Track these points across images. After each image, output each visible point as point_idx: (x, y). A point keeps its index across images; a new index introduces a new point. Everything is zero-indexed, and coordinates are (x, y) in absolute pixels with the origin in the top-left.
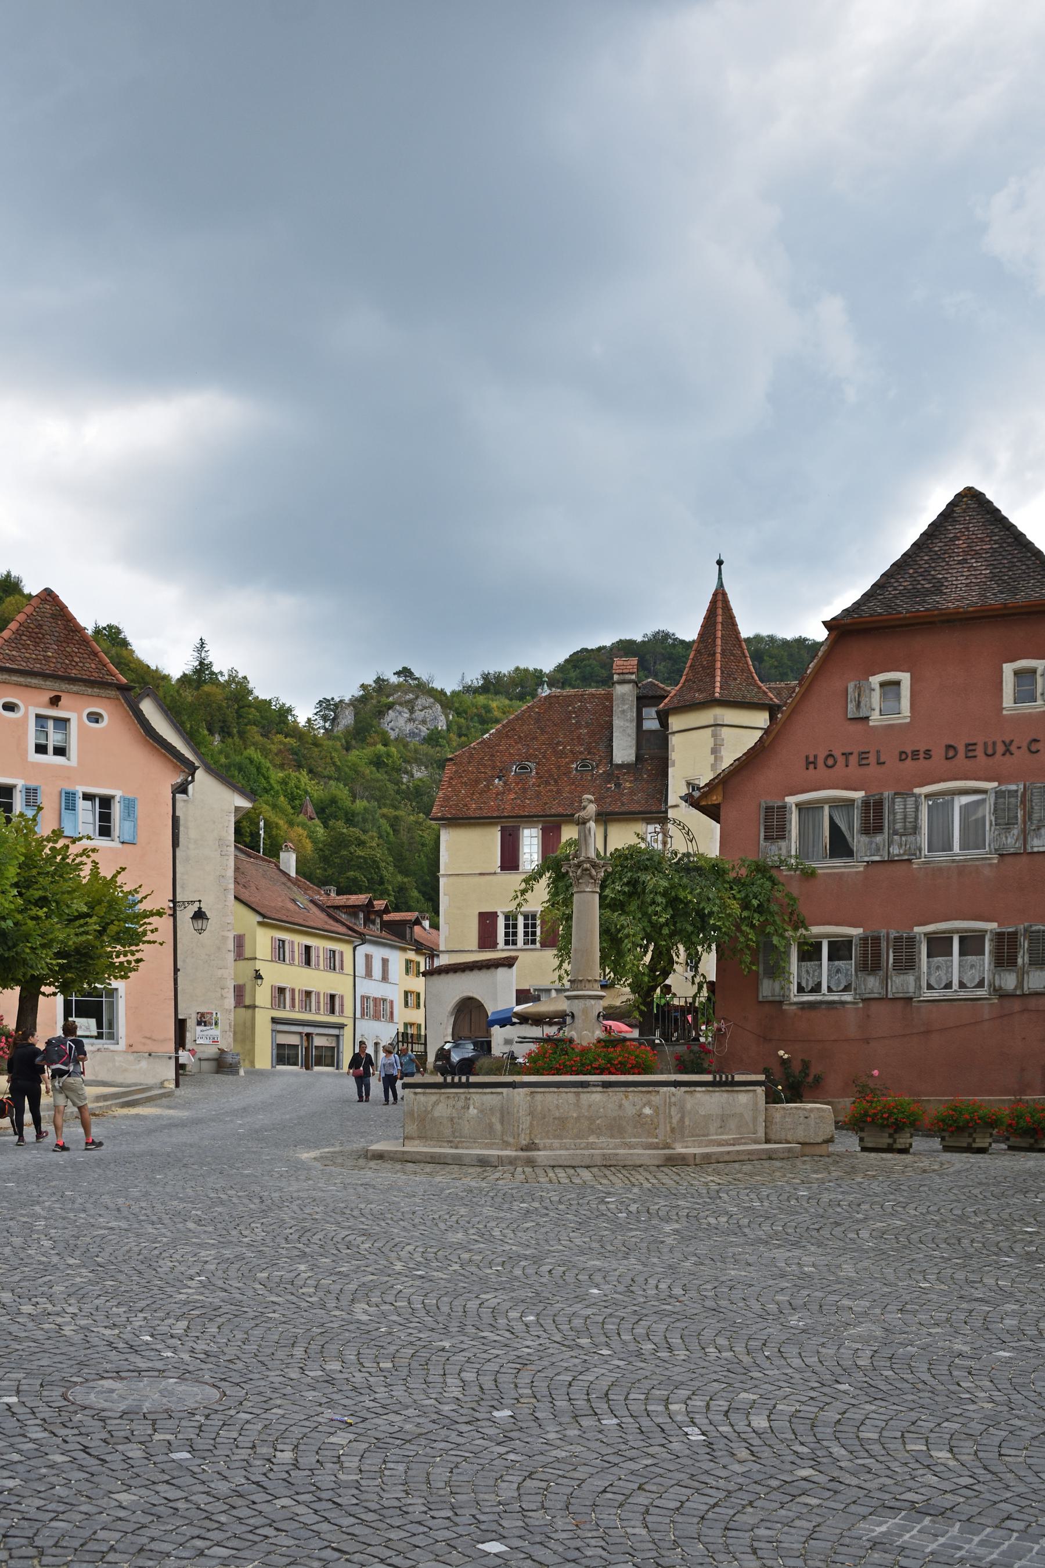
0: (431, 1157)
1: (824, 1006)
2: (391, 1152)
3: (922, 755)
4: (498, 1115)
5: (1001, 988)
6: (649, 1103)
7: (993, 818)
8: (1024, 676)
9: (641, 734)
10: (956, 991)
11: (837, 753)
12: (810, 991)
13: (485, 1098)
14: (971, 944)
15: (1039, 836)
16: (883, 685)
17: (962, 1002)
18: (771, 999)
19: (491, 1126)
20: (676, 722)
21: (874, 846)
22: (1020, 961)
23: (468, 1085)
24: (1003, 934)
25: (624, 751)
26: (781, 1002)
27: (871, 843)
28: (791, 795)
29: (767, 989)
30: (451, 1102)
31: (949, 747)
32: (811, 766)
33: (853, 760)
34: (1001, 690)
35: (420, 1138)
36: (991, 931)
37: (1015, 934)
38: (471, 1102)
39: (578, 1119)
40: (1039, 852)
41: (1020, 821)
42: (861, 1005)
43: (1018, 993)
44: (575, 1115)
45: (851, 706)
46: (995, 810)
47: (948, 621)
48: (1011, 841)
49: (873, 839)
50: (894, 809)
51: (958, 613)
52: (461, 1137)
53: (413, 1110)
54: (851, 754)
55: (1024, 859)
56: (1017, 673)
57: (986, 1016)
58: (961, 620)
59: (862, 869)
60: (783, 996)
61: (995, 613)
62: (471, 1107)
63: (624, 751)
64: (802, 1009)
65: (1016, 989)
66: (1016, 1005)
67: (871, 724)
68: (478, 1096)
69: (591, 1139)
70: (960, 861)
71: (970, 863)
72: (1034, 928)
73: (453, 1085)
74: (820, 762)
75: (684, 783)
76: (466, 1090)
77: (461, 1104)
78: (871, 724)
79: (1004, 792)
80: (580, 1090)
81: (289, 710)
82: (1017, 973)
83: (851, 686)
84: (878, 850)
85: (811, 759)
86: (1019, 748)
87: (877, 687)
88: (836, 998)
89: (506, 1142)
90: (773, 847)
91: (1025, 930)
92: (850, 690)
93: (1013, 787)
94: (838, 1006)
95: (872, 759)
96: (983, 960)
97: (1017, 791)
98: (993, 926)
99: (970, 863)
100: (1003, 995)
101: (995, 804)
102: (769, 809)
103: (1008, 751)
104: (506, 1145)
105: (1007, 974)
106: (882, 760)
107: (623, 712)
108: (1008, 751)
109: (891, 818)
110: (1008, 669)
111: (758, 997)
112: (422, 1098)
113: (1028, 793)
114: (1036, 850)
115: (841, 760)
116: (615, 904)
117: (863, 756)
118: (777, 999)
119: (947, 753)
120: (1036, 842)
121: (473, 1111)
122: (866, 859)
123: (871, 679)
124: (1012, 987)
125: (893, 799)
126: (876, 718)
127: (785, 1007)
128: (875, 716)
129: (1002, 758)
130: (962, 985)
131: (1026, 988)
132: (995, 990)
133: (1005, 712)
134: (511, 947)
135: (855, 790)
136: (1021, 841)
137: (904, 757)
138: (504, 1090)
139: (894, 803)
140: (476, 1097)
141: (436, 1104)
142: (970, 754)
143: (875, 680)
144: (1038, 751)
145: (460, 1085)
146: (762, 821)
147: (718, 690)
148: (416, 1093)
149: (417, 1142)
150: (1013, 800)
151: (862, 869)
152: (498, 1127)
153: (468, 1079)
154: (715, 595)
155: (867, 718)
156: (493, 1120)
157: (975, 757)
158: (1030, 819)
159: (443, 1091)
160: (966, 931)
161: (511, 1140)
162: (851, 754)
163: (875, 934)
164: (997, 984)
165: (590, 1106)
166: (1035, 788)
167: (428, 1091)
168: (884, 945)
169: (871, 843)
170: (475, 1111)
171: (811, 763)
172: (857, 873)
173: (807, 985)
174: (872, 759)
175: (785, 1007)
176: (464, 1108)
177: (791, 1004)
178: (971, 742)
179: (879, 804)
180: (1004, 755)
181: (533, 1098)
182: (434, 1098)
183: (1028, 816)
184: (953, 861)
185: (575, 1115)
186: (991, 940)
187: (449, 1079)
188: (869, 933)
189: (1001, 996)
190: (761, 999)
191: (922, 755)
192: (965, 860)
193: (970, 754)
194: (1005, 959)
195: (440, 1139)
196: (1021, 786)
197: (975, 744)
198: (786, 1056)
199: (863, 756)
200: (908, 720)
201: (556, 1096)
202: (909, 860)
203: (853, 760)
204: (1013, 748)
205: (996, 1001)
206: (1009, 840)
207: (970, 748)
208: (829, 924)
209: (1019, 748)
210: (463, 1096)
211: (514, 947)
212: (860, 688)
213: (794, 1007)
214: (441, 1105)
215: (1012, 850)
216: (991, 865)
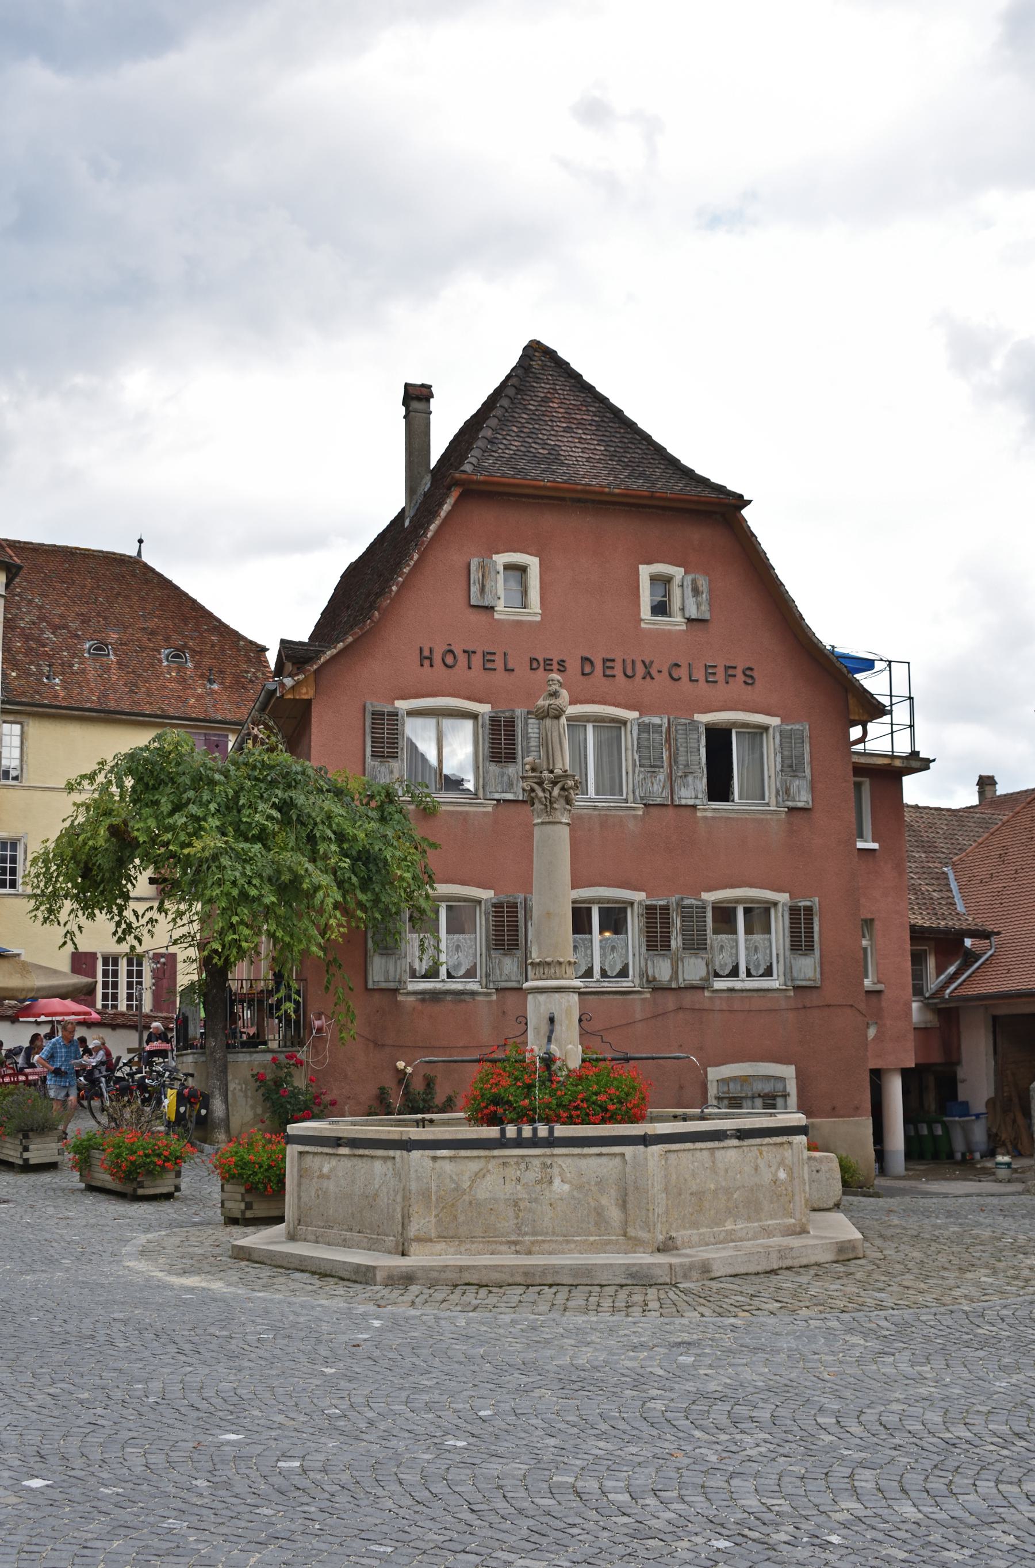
0: (526, 1274)
1: (449, 998)
2: (432, 1268)
4: (613, 1192)
5: (655, 979)
6: (782, 1163)
7: (636, 757)
10: (598, 981)
11: (458, 652)
12: (423, 977)
13: (583, 1163)
14: (614, 919)
15: (686, 785)
16: (508, 567)
17: (611, 997)
18: (383, 985)
19: (599, 1212)
21: (505, 778)
22: (673, 943)
23: (551, 1142)
26: (395, 991)
27: (502, 775)
28: (403, 699)
29: (379, 970)
30: (512, 1172)
31: (586, 660)
32: (427, 663)
33: (477, 660)
34: (638, 597)
35: (441, 1237)
36: (640, 903)
37: (666, 908)
38: (556, 1171)
39: (715, 1191)
40: (686, 806)
41: (665, 764)
42: (494, 997)
43: (674, 986)
44: (712, 1187)
45: (475, 589)
46: (639, 747)
47: (579, 500)
48: (657, 789)
49: (505, 770)
50: (528, 733)
51: (602, 493)
52: (534, 1234)
53: (429, 1189)
54: (474, 652)
55: (671, 811)
56: (654, 579)
57: (638, 1016)
58: (593, 501)
59: (490, 809)
60: (400, 982)
61: (667, 504)
62: (557, 1181)
64: (423, 1000)
65: (670, 981)
66: (670, 1002)
67: (496, 616)
68: (569, 1160)
69: (729, 1226)
70: (603, 808)
71: (613, 813)
72: (686, 902)
73: (519, 1142)
74: (437, 658)
76: (547, 1151)
77: (531, 1176)
78: (496, 616)
79: (648, 725)
80: (716, 1144)
81: (741, 502)
82: (672, 959)
83: (474, 563)
84: (511, 785)
85: (426, 653)
86: (659, 672)
87: (501, 569)
88: (459, 987)
89: (635, 1239)
90: (383, 769)
91: (677, 904)
92: (473, 568)
93: (656, 720)
94: (467, 998)
95: (499, 664)
96: (736, 941)
97: (661, 726)
98: (639, 896)
99: (613, 813)
100: (658, 988)
101: (639, 739)
102: (377, 715)
104: (635, 1244)
105: (661, 959)
106: (510, 667)
108: (648, 675)
109: (524, 744)
110: (645, 571)
111: (366, 982)
112: (448, 1167)
113: (673, 729)
114: (683, 802)
115: (462, 659)
116: (240, 835)
117: (488, 657)
118: (392, 985)
120: (684, 793)
121: (560, 1187)
122: (497, 796)
123: (495, 557)
124: (667, 978)
125: (526, 719)
126: (502, 611)
127: (400, 998)
128: (500, 606)
130: (604, 974)
131: (681, 980)
132: (648, 981)
133: (643, 625)
135: (480, 701)
136: (668, 790)
137: (535, 665)
138: (628, 1150)
139: (527, 724)
140: (566, 1163)
141: (477, 1176)
142: (489, 665)
143: (502, 559)
144: (422, 665)
145: (535, 1142)
146: (368, 730)
148: (435, 1158)
149: (440, 1246)
150: (657, 736)
151: (490, 809)
152: (614, 1214)
153: (551, 1131)
155: (492, 608)
156: (604, 1201)
157: (614, 676)
158: (676, 762)
159: (496, 1152)
160: (609, 901)
161: (643, 1235)
162: (474, 652)
163: (511, 899)
164: (650, 973)
165: (727, 1171)
166: (679, 724)
167: (463, 1153)
169: (502, 775)
170: (566, 1187)
171: (426, 658)
172: (486, 813)
173: (420, 966)
174: (499, 664)
175: (400, 998)
176: (539, 1182)
177: (409, 993)
178: (609, 657)
179: (511, 723)
180: (644, 678)
181: (667, 1159)
182: (474, 1166)
183: (673, 758)
184: (595, 808)
185: (712, 1187)
186: (640, 915)
187: (527, 1131)
188: (503, 898)
190: (370, 986)
192: (609, 808)
194: (656, 941)
195: (490, 1238)
196: (666, 721)
197: (613, 660)
198: (409, 1070)
199: (488, 657)
200: (538, 618)
201: (689, 1155)
202: (694, 806)
203: (477, 660)
205: (648, 996)
206: (656, 787)
207: (489, 657)
209: (659, 672)
210: (537, 1162)
211: (12, 891)
212: (483, 567)
213: (412, 998)
214: (488, 1178)
215: (659, 801)
216: (635, 817)
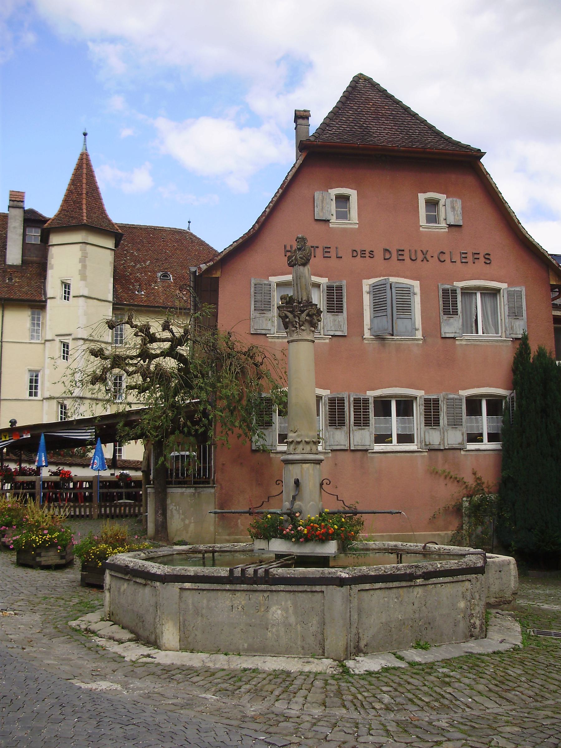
3: (367, 255)
8: (432, 204)
9: (25, 247)
20: (54, 239)
24: (429, 400)
25: (14, 256)
31: (386, 250)
36: (420, 398)
59: (327, 341)
63: (14, 256)
67: (331, 225)
75: (60, 282)
95: (333, 254)
99: (403, 342)
103: (425, 259)
106: (339, 256)
107: (15, 228)
110: (422, 197)
119: (384, 255)
129: (421, 263)
131: (446, 444)
132: (426, 445)
134: (33, 398)
147: (85, 218)
154: (82, 155)
155: (329, 220)
160: (402, 396)
164: (427, 440)
168: (346, 404)
189: (430, 450)
191: (367, 255)
193: (401, 258)
197: (403, 250)
200: (357, 226)
204: (428, 257)
208: (473, 387)
216: (418, 345)
